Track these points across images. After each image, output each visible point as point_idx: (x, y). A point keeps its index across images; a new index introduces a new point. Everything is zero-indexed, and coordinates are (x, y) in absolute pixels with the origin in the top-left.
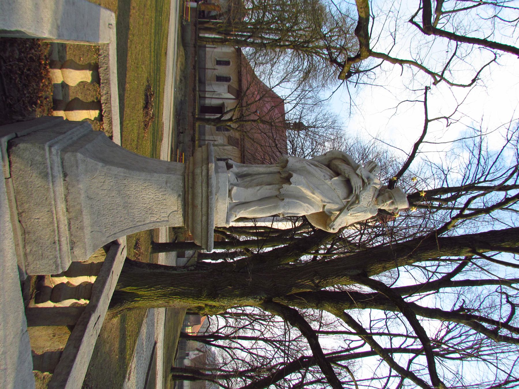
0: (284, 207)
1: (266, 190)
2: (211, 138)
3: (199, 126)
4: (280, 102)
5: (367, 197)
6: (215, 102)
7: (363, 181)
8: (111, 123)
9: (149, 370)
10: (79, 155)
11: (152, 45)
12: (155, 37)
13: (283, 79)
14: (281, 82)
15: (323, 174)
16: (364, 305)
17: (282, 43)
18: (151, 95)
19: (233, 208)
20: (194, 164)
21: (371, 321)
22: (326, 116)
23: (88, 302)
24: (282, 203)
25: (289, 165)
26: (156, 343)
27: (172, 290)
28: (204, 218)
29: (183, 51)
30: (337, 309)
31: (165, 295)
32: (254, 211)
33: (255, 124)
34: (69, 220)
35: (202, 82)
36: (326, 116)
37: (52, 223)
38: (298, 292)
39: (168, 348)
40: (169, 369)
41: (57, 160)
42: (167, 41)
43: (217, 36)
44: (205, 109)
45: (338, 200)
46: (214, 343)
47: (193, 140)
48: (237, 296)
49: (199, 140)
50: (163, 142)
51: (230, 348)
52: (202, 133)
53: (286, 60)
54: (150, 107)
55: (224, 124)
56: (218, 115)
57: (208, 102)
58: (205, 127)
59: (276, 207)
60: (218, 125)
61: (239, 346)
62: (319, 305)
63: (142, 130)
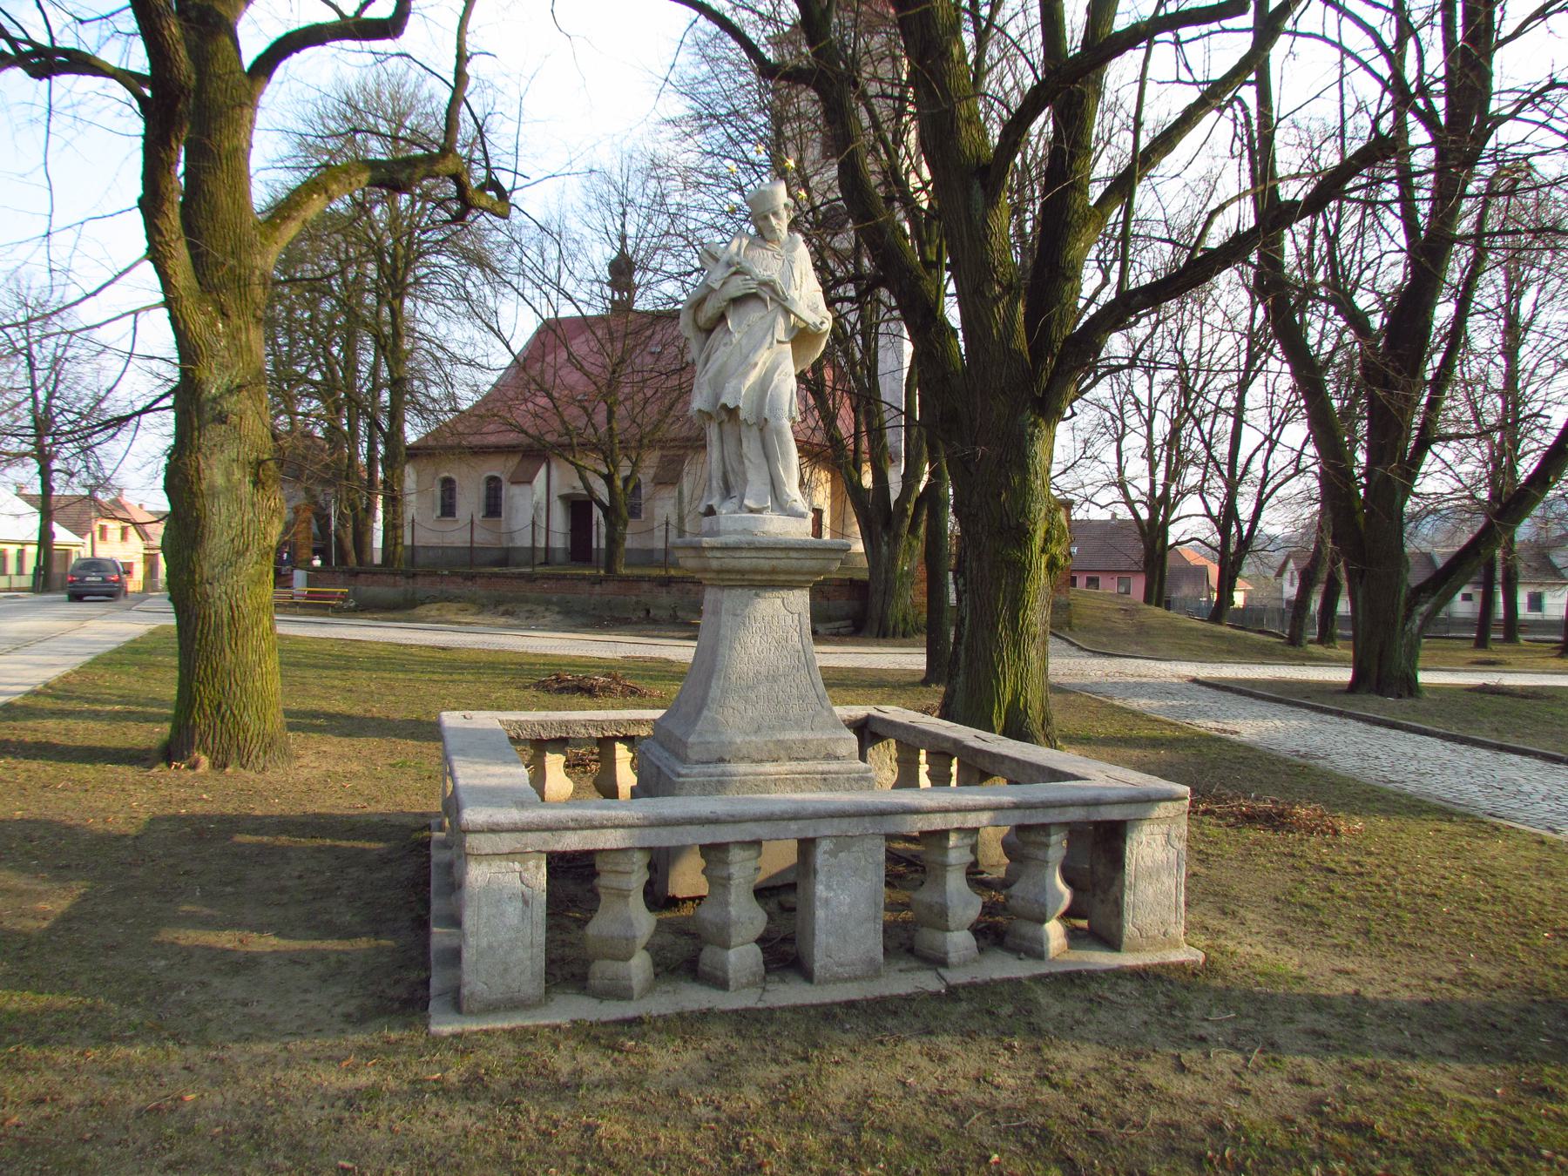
0: (779, 419)
1: (751, 448)
2: (659, 533)
3: (627, 565)
4: (552, 332)
5: (766, 265)
6: (560, 519)
7: (735, 273)
8: (638, 722)
9: (1251, 695)
10: (692, 739)
11: (435, 677)
12: (413, 671)
13: (492, 329)
14: (499, 334)
15: (722, 348)
16: (1081, 152)
17: (387, 330)
18: (558, 680)
19: (781, 505)
20: (705, 570)
21: (1178, 81)
22: (593, 202)
23: (955, 761)
24: (772, 421)
25: (705, 408)
26: (1195, 681)
27: (1005, 627)
28: (793, 554)
29: (428, 607)
30: (1085, 225)
31: (1016, 644)
32: (787, 468)
33: (621, 411)
34: (790, 759)
35: (506, 557)
36: (593, 202)
37: (793, 781)
38: (1023, 335)
39: (1229, 652)
40: (1291, 650)
41: (698, 769)
42: (412, 646)
43: (380, 514)
44: (580, 546)
45: (769, 319)
46: (1246, 528)
47: (667, 582)
48: (1025, 482)
49: (665, 565)
50: (672, 658)
51: (1264, 483)
52: (647, 557)
53: (435, 321)
54: (588, 683)
55: (621, 498)
56: (597, 513)
57: (559, 541)
58: (628, 550)
59: (779, 433)
60: (625, 512)
61: (1260, 456)
62: (1069, 273)
63: (646, 701)
